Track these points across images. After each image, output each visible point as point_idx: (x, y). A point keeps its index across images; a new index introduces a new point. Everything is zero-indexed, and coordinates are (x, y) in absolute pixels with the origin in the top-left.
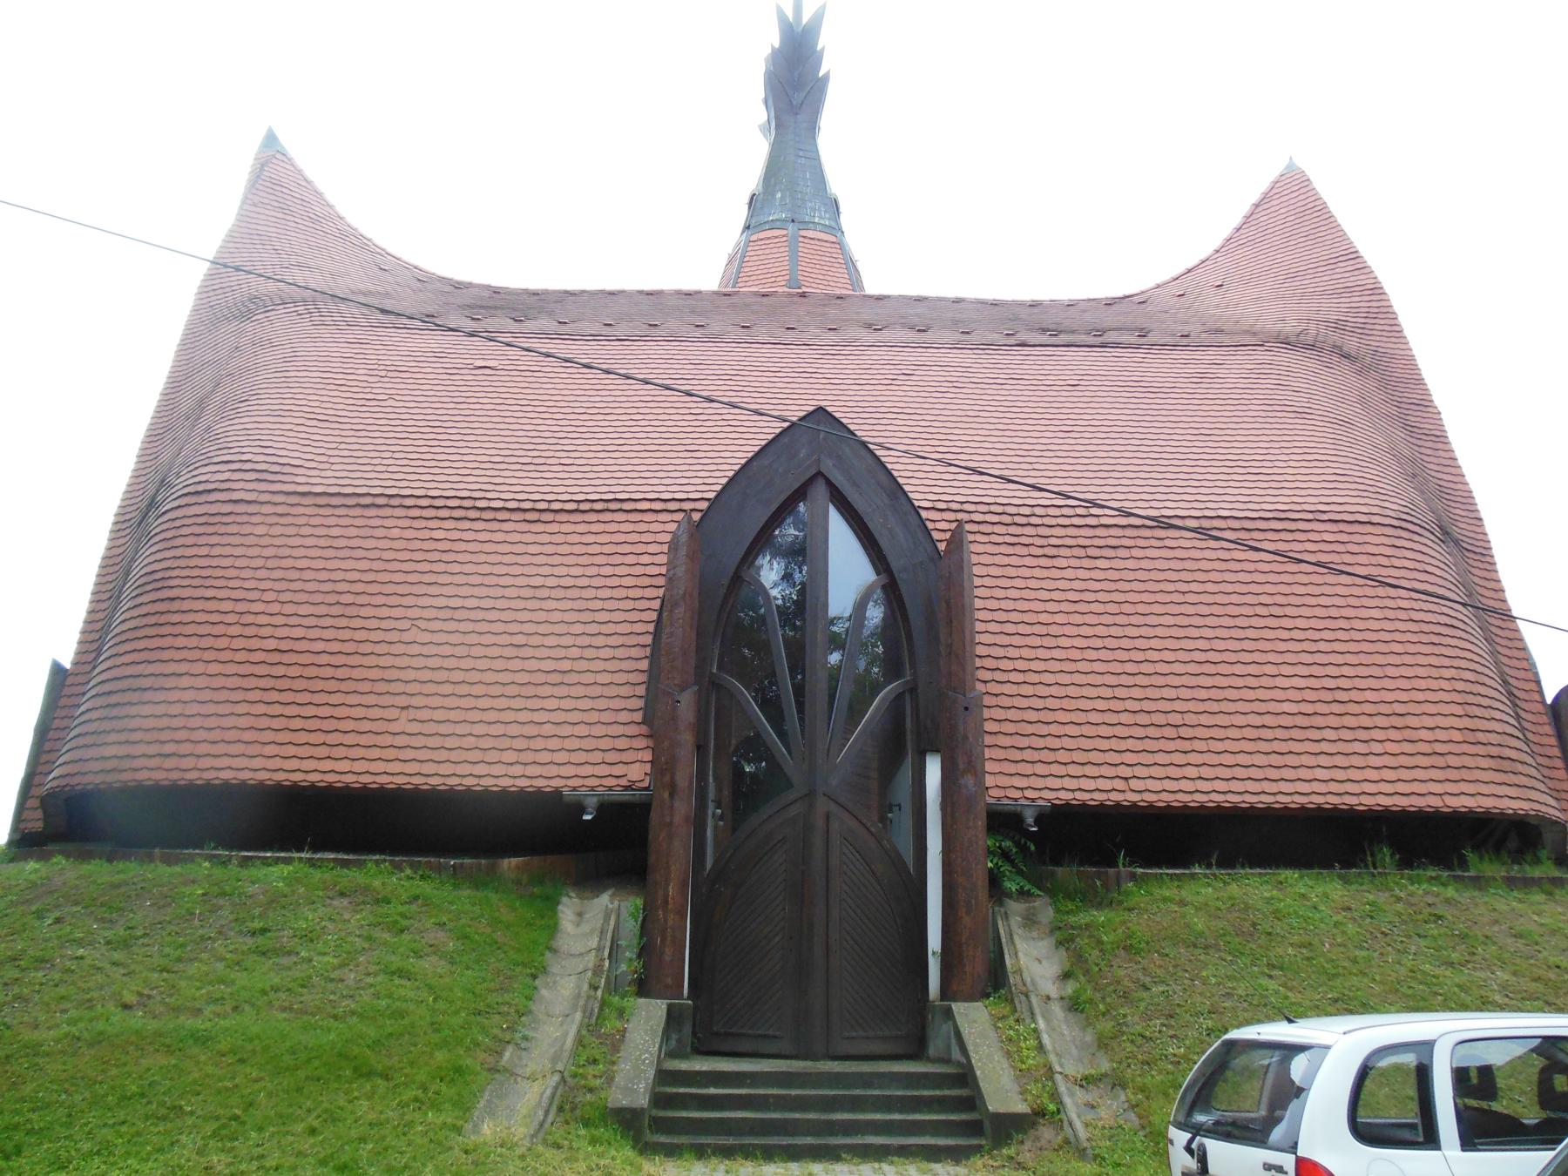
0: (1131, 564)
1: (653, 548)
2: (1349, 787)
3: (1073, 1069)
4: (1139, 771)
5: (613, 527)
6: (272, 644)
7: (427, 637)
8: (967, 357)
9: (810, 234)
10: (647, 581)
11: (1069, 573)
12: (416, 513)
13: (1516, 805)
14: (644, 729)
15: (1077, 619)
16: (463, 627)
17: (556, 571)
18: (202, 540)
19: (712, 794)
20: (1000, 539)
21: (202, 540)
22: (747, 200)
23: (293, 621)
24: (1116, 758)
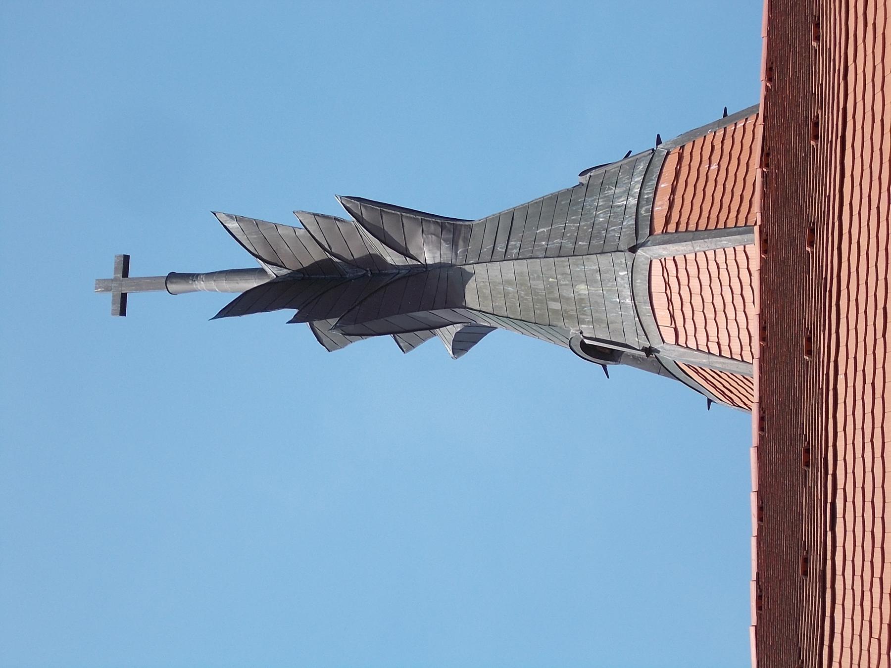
9: (661, 208)
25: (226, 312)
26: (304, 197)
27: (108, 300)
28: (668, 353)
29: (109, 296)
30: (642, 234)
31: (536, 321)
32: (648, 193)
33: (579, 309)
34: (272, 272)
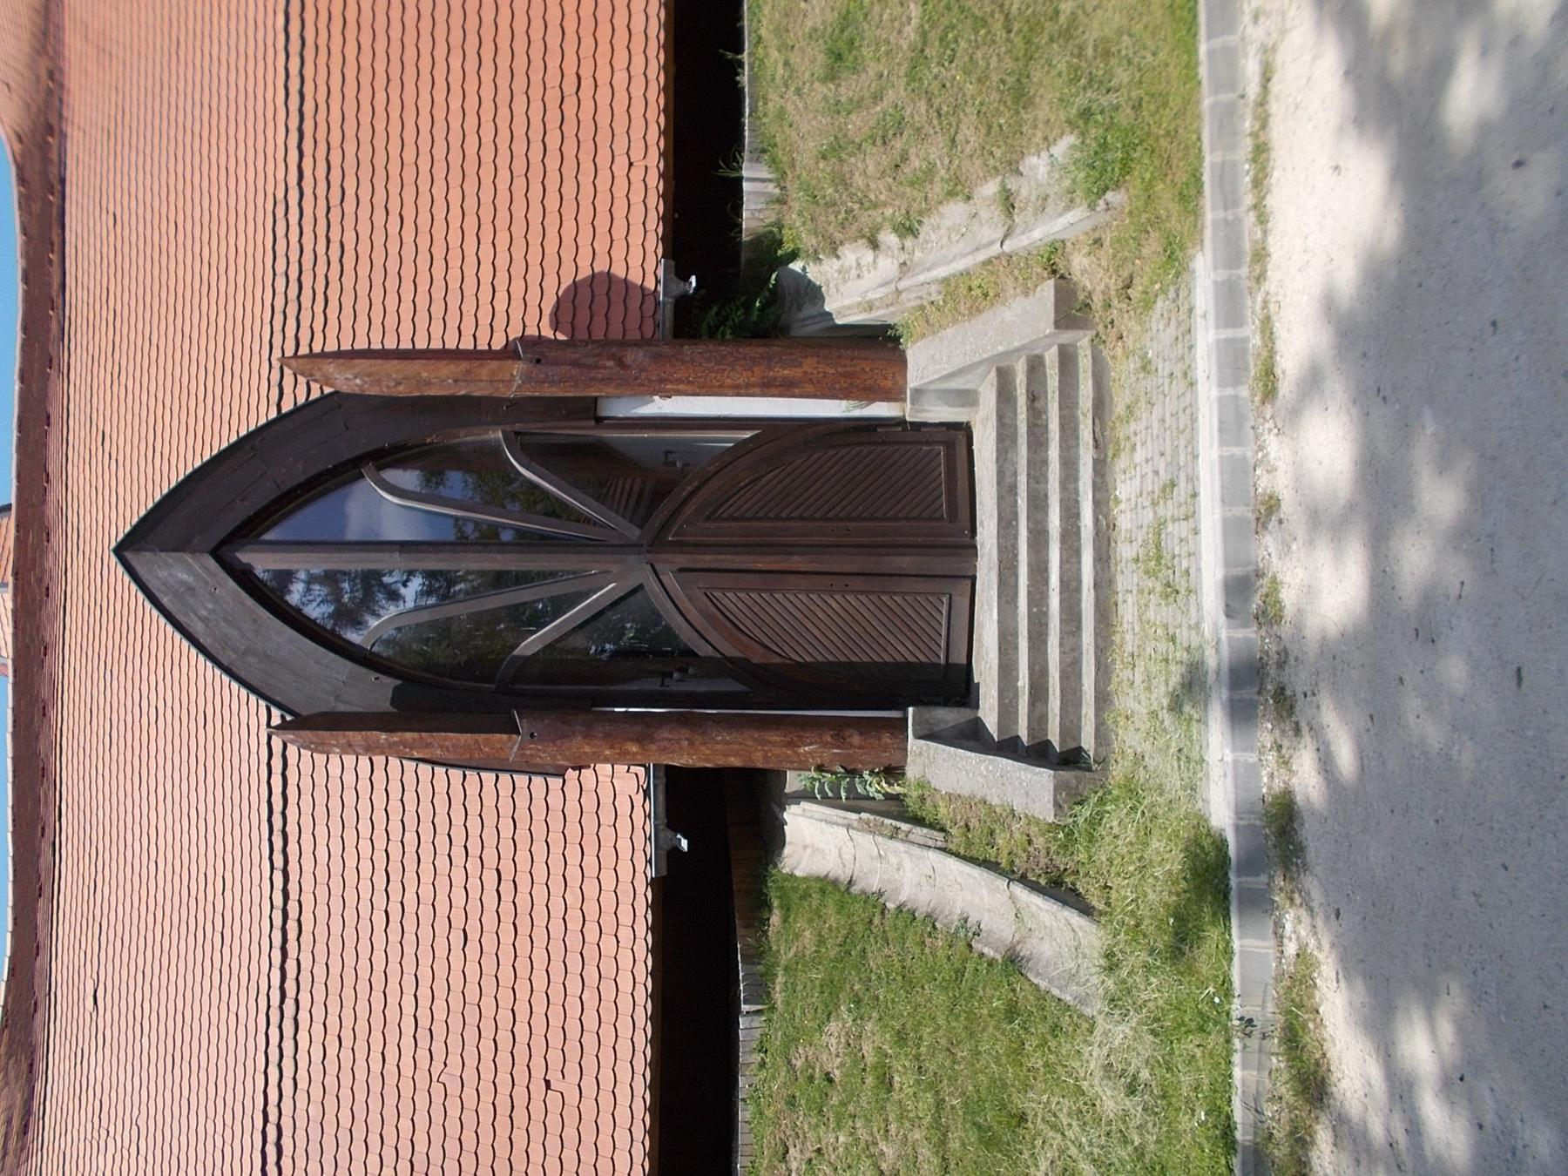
0: (350, 148)
3: (989, 230)
4: (621, 145)
7: (454, 1060)
10: (379, 775)
14: (571, 774)
15: (424, 219)
16: (440, 1015)
17: (365, 895)
19: (652, 685)
24: (604, 175)
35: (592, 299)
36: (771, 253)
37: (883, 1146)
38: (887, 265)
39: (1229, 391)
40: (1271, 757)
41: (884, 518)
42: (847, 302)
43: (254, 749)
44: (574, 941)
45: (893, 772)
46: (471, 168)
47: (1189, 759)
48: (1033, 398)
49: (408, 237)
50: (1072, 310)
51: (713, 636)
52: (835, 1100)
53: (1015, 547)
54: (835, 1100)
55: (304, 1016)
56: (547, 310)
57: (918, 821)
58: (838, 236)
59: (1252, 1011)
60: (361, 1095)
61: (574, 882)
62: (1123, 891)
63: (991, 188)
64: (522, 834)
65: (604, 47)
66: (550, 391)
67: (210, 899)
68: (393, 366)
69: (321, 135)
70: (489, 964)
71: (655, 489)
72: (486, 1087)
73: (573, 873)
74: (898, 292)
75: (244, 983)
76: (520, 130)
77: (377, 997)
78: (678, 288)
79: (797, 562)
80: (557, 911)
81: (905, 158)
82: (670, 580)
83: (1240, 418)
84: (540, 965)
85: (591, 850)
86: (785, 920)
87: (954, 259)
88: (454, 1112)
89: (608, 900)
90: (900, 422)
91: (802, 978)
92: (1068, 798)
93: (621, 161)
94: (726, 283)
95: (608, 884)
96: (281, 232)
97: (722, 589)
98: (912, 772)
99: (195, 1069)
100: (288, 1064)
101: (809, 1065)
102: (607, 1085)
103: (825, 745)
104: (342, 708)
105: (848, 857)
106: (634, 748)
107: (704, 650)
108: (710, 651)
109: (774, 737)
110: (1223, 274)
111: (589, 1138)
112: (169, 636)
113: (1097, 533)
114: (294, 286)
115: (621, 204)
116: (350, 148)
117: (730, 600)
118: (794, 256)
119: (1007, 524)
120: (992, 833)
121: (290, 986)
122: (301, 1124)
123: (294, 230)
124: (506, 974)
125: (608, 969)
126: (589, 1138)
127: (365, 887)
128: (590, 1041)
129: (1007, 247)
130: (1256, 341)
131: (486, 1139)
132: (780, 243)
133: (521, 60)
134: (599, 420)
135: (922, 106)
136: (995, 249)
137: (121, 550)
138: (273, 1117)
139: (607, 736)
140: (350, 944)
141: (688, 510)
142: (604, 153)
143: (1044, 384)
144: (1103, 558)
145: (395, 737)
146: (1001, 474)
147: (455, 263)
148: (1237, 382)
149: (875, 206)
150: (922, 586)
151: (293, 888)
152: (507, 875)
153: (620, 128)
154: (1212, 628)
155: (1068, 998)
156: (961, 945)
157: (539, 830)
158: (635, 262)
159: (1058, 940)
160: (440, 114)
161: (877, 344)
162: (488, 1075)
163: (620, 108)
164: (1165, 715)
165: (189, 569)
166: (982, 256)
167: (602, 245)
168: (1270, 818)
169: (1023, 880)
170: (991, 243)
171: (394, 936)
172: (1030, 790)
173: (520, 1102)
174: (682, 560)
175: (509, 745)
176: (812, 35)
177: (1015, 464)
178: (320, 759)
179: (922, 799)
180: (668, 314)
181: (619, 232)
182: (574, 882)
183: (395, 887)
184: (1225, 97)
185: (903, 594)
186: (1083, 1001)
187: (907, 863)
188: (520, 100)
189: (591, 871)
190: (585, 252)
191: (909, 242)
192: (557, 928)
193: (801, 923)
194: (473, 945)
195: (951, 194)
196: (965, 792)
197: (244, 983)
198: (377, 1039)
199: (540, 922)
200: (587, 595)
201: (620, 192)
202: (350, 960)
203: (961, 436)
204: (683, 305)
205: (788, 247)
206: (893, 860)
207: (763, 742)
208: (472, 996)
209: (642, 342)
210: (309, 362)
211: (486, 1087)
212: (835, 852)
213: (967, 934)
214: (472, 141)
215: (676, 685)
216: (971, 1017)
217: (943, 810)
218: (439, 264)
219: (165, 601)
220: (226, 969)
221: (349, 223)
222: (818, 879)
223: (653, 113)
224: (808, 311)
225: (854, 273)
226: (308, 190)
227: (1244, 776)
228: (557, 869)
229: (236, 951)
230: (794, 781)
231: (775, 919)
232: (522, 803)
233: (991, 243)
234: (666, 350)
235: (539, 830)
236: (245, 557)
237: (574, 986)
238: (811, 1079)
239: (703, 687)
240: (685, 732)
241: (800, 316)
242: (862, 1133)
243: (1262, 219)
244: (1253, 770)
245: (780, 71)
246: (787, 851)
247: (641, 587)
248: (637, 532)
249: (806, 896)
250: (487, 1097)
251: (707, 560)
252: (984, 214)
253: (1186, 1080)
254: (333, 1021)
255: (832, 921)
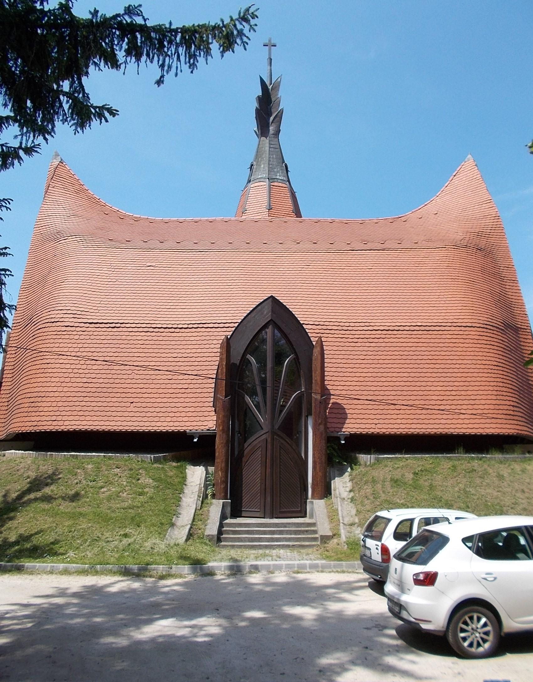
0: (383, 345)
1: (215, 342)
2: (452, 426)
3: (347, 520)
5: (201, 334)
6: (85, 380)
7: (138, 377)
8: (331, 256)
9: (276, 184)
10: (213, 354)
11: (360, 349)
12: (131, 329)
13: (509, 431)
14: (213, 409)
17: (181, 351)
18: (56, 341)
20: (337, 336)
21: (56, 341)
22: (252, 106)
23: (91, 371)
24: (374, 417)
25: (261, 79)
26: (286, 100)
27: (267, 41)
28: (249, 184)
29: (268, 42)
30: (271, 180)
31: (258, 154)
32: (279, 181)
33: (259, 165)
34: (270, 87)
35: (341, 414)
36: (353, 462)
37: (125, 493)
38: (345, 494)
39: (296, 566)
40: (223, 573)
41: (280, 494)
42: (337, 484)
43: (220, 318)
44: (169, 410)
45: (214, 496)
46: (376, 379)
47: (221, 560)
48: (307, 531)
49: (358, 361)
50: (325, 539)
51: (249, 448)
52: (134, 481)
53: (271, 527)
54: (134, 481)
55: (149, 334)
56: (337, 401)
57: (202, 503)
58: (354, 481)
59: (174, 569)
60: (128, 350)
61: (185, 410)
62: (192, 548)
63: (357, 520)
64: (197, 395)
65: (408, 417)
66: (313, 405)
67: (179, 304)
68: (319, 361)
69: (387, 336)
70: (163, 386)
71: (290, 429)
72: (131, 386)
73: (187, 409)
74: (337, 497)
75: (157, 316)
76: (386, 393)
77: (155, 355)
78: (342, 438)
79: (268, 470)
80: (177, 405)
81: (368, 499)
82: (264, 437)
83: (291, 568)
84: (163, 400)
85: (194, 414)
86: (175, 467)
87: (342, 511)
88: (124, 377)
89: (180, 419)
90: (307, 498)
91: (161, 472)
92: (210, 537)
93: (377, 422)
94: (344, 450)
95: (184, 419)
96: (361, 324)
97: (261, 451)
98: (214, 501)
99: (133, 300)
100: (136, 329)
101: (141, 474)
102: (133, 419)
103: (221, 478)
104: (232, 350)
105: (192, 484)
106: (221, 428)
107: (246, 445)
108: (246, 447)
109: (223, 465)
110: (320, 565)
111: (118, 414)
112: (251, 306)
113: (272, 545)
114: (346, 328)
115: (366, 421)
116: (383, 345)
117: (259, 453)
118: (352, 469)
119: (276, 525)
120: (201, 520)
121: (157, 330)
122: (120, 334)
123: (362, 328)
124: (161, 391)
125: (162, 419)
126: (118, 414)
127: (183, 351)
128: (143, 414)
129: (341, 524)
130: (306, 571)
131: (117, 386)
132: (355, 465)
133: (405, 393)
134: (307, 416)
135: (378, 503)
136: (341, 521)
137: (272, 298)
138: (122, 325)
139: (224, 421)
140: (168, 347)
141: (282, 441)
142: (380, 417)
143: (310, 534)
144: (266, 547)
145: (224, 366)
146: (289, 524)
147: (351, 375)
148: (298, 567)
149: (359, 492)
150: (262, 504)
151: (183, 330)
152: (186, 391)
153: (386, 421)
154: (248, 563)
155: (167, 536)
156: (174, 513)
157: (199, 400)
158: (350, 426)
159: (179, 534)
160: (391, 370)
161: (326, 491)
162: (134, 386)
163: (391, 421)
164: (230, 557)
165: (267, 314)
166: (341, 518)
167: (355, 416)
168: (211, 572)
169: (191, 527)
170: (343, 520)
171: (170, 359)
172: (212, 529)
173: (127, 395)
174: (269, 440)
175: (221, 396)
176: (403, 475)
177: (292, 527)
178: (219, 346)
179: (208, 504)
180: (335, 435)
181: (358, 421)
182: (185, 410)
183: (183, 359)
184: (357, 566)
185: (260, 499)
186: (167, 540)
187: (192, 500)
188: (395, 393)
189: (188, 414)
190: (353, 411)
191: (349, 500)
192: (173, 405)
193: (174, 472)
194: (168, 381)
195: (357, 511)
196: (210, 514)
197: (157, 316)
198: (144, 355)
199: (174, 400)
200: (261, 415)
201: (369, 421)
202: (164, 347)
203: (303, 515)
204: (338, 439)
205: (354, 467)
206: (192, 496)
207: (222, 462)
208: (155, 382)
209: (326, 428)
210: (320, 342)
211: (131, 386)
212: (193, 480)
213: (177, 514)
214: (384, 379)
215: (237, 436)
216: (159, 515)
217: (205, 509)
218: (351, 370)
219: (259, 307)
220: (160, 310)
221: (363, 344)
222: (186, 476)
223: (389, 430)
224: (337, 473)
225: (345, 485)
226: (372, 332)
227: (219, 568)
228: (188, 405)
229: (165, 313)
230: (211, 469)
231: (174, 464)
232: (206, 395)
233: (343, 520)
234: (324, 436)
235: (199, 400)
236: (270, 327)
237: (158, 410)
238: (138, 475)
239: (236, 444)
240: (225, 442)
241: (336, 471)
242: (127, 488)
243: (330, 572)
244: (220, 570)
245: (396, 466)
246: (192, 467)
247: (262, 429)
248: (277, 428)
249: (182, 473)
250: (128, 386)
251: (269, 446)
252: (351, 519)
253: (157, 558)
254: (148, 342)
255: (176, 480)
